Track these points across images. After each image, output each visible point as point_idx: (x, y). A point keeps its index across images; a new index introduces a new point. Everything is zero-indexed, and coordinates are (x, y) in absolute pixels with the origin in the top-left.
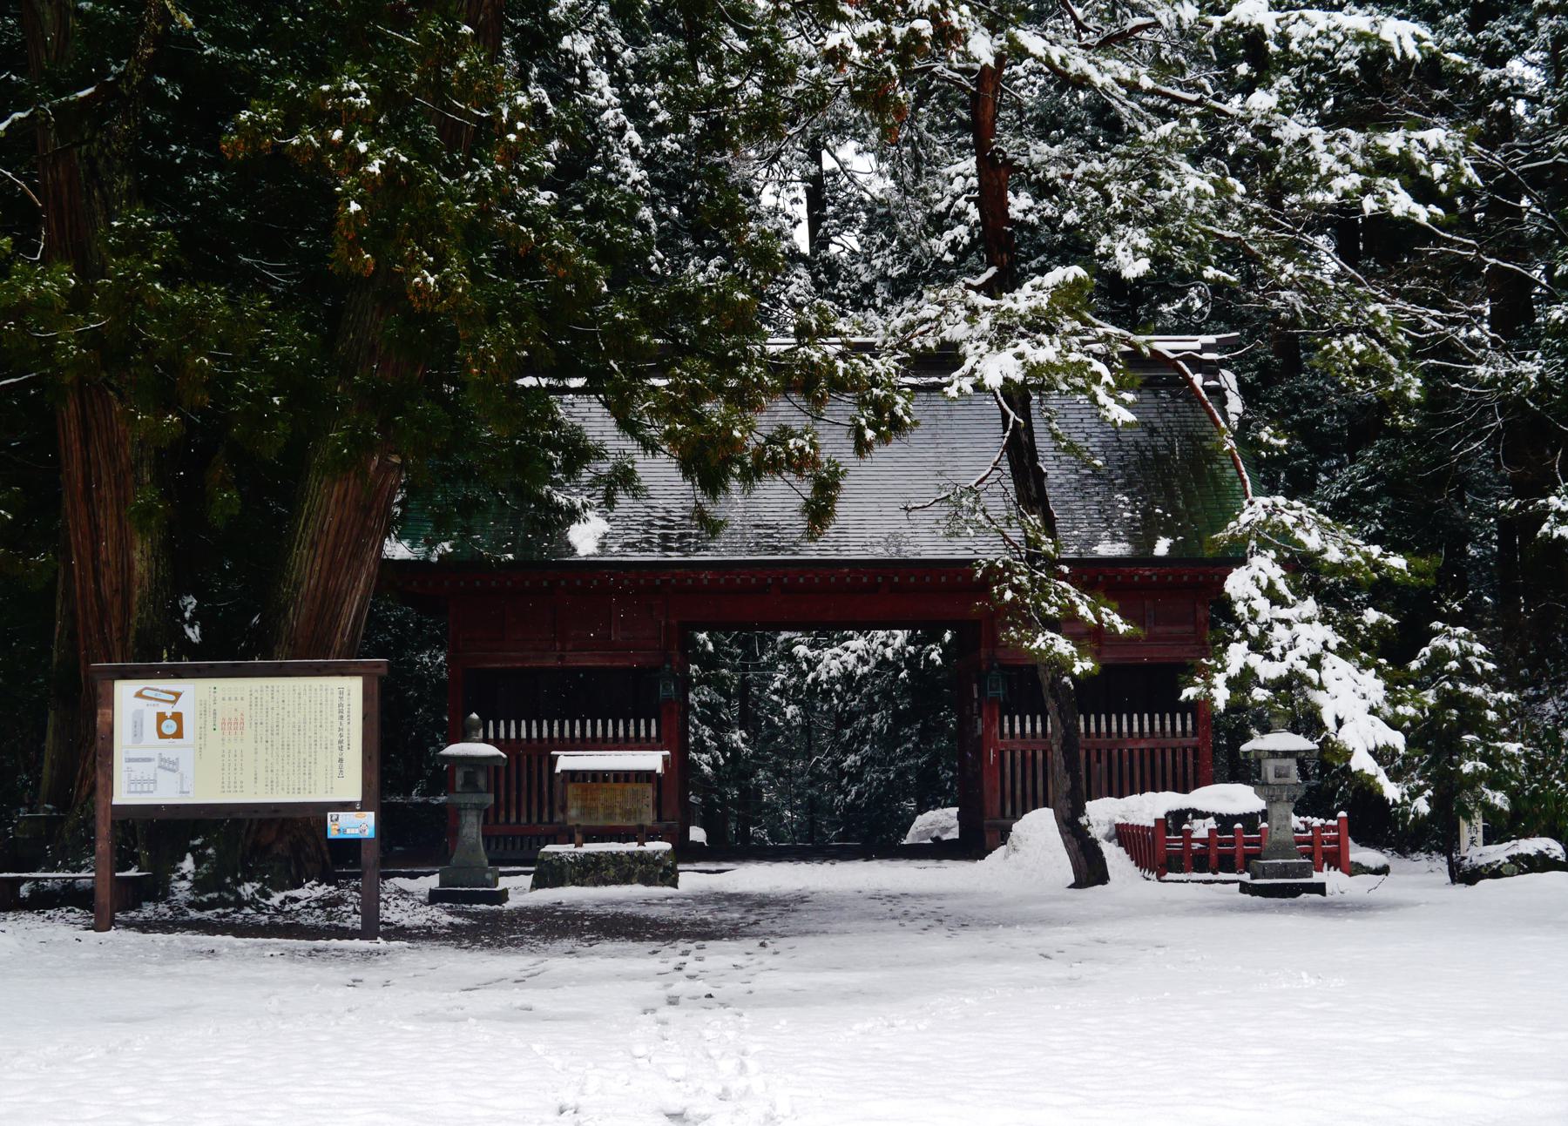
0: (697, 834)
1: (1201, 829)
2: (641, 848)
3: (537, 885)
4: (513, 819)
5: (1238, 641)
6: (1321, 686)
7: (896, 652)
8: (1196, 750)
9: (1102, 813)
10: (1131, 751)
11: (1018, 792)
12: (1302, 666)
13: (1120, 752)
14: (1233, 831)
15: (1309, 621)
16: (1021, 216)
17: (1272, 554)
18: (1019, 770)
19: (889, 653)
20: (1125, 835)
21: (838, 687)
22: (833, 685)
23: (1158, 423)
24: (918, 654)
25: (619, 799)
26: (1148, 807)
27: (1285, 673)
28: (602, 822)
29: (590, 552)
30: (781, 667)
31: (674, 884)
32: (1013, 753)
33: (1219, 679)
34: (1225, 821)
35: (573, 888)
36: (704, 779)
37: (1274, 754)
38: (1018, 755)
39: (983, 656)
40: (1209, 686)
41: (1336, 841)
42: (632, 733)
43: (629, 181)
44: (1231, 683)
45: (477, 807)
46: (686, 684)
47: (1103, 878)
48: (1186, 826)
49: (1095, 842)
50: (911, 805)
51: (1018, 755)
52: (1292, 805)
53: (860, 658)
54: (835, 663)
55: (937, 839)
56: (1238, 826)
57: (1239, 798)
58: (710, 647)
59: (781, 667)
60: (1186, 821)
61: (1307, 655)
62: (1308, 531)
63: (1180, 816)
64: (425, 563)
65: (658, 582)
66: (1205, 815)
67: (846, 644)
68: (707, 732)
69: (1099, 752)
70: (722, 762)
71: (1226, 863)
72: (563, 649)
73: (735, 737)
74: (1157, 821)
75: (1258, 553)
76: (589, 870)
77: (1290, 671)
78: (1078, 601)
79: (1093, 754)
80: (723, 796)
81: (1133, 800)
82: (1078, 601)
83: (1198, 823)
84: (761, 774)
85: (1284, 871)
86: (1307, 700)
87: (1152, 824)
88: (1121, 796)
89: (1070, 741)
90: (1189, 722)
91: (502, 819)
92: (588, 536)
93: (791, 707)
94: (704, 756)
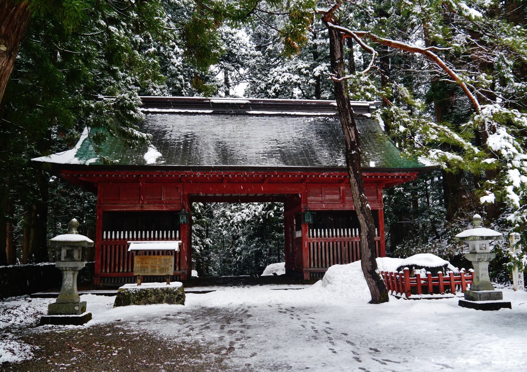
0: (194, 273)
2: (168, 286)
3: (118, 303)
4: (121, 270)
7: (259, 213)
8: (379, 242)
11: (316, 258)
13: (352, 242)
16: (296, 81)
21: (240, 224)
24: (266, 214)
25: (158, 263)
29: (152, 163)
35: (134, 306)
36: (197, 254)
38: (315, 244)
39: (302, 207)
45: (74, 269)
46: (191, 223)
50: (52, 234)
51: (315, 244)
53: (247, 215)
54: (239, 217)
58: (199, 211)
64: (84, 165)
65: (180, 176)
67: (243, 211)
68: (198, 239)
69: (345, 242)
70: (203, 249)
76: (143, 297)
79: (343, 243)
80: (203, 259)
84: (212, 253)
85: (490, 296)
91: (117, 270)
92: (152, 157)
93: (225, 231)
94: (197, 247)
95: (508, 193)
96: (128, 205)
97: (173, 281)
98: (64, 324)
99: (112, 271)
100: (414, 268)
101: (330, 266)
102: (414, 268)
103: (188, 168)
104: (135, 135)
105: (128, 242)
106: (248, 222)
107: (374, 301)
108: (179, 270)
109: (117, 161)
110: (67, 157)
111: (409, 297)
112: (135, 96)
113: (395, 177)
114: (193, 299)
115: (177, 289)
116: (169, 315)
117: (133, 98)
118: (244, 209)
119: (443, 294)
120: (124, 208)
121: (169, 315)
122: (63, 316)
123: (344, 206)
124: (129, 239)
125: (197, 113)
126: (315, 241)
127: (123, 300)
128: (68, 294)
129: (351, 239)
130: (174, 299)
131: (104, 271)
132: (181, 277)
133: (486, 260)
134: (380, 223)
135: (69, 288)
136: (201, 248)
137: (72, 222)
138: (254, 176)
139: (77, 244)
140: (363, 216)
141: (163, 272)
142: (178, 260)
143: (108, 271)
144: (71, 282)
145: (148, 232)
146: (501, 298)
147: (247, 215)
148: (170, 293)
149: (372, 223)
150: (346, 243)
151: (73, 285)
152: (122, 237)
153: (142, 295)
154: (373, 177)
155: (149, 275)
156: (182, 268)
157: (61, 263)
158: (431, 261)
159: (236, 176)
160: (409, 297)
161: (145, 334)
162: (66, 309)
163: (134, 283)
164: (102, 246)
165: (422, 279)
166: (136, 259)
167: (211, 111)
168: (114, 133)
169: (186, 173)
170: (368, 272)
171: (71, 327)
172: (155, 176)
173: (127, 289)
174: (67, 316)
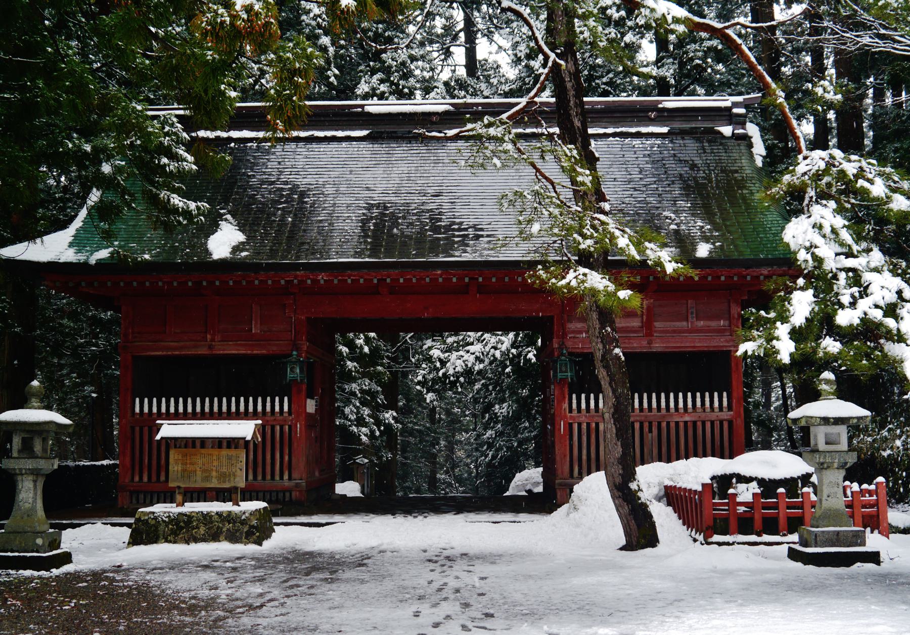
1: (745, 493)
2: (236, 509)
3: (136, 539)
5: (802, 289)
6: (900, 338)
7: (503, 354)
8: (730, 423)
9: (651, 477)
10: (677, 423)
11: (584, 457)
12: (877, 315)
13: (668, 423)
14: (776, 496)
15: (877, 270)
17: (832, 204)
18: (584, 438)
19: (498, 354)
20: (673, 496)
21: (462, 379)
22: (458, 378)
23: (698, 161)
24: (519, 355)
26: (696, 472)
27: (856, 321)
28: (200, 484)
30: (424, 366)
31: (260, 545)
32: (580, 425)
33: (782, 330)
34: (768, 486)
35: (166, 545)
37: (826, 421)
38: (584, 426)
40: (770, 338)
41: (876, 504)
42: (268, 408)
43: (312, 15)
44: (796, 334)
47: (653, 541)
48: (731, 491)
49: (644, 507)
51: (584, 426)
52: (842, 473)
53: (477, 358)
55: (529, 491)
56: (781, 490)
57: (779, 464)
58: (366, 349)
59: (424, 366)
60: (730, 486)
61: (882, 303)
62: (871, 182)
63: (724, 482)
64: (85, 265)
65: (283, 282)
66: (748, 480)
69: (650, 423)
70: (378, 433)
71: (771, 526)
72: (213, 340)
73: (387, 415)
74: (704, 485)
75: (817, 202)
76: (182, 528)
77: (862, 320)
78: (617, 233)
79: (646, 425)
81: (680, 465)
82: (617, 233)
83: (742, 487)
85: (837, 539)
86: (885, 356)
87: (700, 488)
88: (669, 461)
89: (621, 413)
90: (725, 400)
93: (430, 395)
94: (364, 429)
95: (778, 339)
96: (182, 343)
97: (244, 499)
98: (17, 569)
99: (154, 479)
100: (734, 480)
101: (589, 473)
102: (734, 480)
103: (295, 267)
104: (174, 205)
105: (158, 422)
106: (480, 372)
107: (630, 546)
108: (290, 478)
109: (147, 257)
110: (55, 247)
111: (710, 540)
112: (172, 125)
113: (762, 278)
114: (287, 536)
115: (247, 515)
116: (217, 561)
117: (167, 128)
118: (472, 344)
119: (784, 535)
120: (176, 349)
121: (217, 561)
122: (16, 554)
123: (650, 343)
124: (160, 415)
125: (334, 139)
126: (584, 419)
127: (144, 534)
128: (25, 517)
129: (664, 416)
130: (241, 533)
131: (137, 479)
132: (293, 494)
133: (836, 465)
134: (734, 383)
135: (27, 505)
136: (372, 432)
137: (32, 387)
138: (440, 280)
139: (38, 428)
140: (605, 373)
141: (224, 482)
142: (287, 458)
143: (145, 479)
144: (31, 495)
145: (224, 400)
146: (863, 544)
147: (477, 358)
148: (235, 522)
149: (624, 387)
150: (655, 424)
151: (35, 501)
152: (146, 410)
153: (182, 524)
154: (710, 278)
155: (197, 486)
156: (295, 475)
157: (12, 461)
158: (775, 466)
159: (401, 280)
160: (710, 540)
161: (147, 585)
162: (21, 543)
163: (171, 502)
164: (133, 428)
165: (741, 504)
166: (173, 455)
167: (364, 133)
168: (133, 201)
169: (296, 277)
170: (615, 486)
171: (28, 573)
172: (231, 283)
173: (153, 513)
174: (22, 554)
